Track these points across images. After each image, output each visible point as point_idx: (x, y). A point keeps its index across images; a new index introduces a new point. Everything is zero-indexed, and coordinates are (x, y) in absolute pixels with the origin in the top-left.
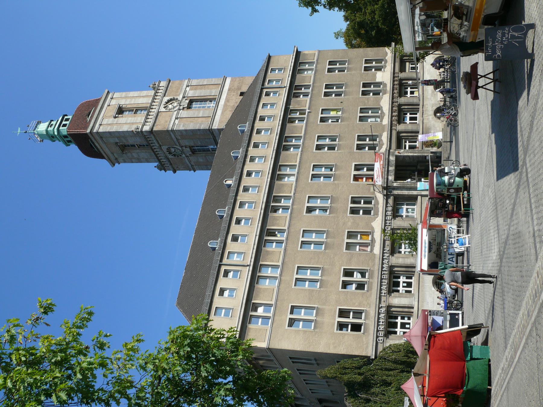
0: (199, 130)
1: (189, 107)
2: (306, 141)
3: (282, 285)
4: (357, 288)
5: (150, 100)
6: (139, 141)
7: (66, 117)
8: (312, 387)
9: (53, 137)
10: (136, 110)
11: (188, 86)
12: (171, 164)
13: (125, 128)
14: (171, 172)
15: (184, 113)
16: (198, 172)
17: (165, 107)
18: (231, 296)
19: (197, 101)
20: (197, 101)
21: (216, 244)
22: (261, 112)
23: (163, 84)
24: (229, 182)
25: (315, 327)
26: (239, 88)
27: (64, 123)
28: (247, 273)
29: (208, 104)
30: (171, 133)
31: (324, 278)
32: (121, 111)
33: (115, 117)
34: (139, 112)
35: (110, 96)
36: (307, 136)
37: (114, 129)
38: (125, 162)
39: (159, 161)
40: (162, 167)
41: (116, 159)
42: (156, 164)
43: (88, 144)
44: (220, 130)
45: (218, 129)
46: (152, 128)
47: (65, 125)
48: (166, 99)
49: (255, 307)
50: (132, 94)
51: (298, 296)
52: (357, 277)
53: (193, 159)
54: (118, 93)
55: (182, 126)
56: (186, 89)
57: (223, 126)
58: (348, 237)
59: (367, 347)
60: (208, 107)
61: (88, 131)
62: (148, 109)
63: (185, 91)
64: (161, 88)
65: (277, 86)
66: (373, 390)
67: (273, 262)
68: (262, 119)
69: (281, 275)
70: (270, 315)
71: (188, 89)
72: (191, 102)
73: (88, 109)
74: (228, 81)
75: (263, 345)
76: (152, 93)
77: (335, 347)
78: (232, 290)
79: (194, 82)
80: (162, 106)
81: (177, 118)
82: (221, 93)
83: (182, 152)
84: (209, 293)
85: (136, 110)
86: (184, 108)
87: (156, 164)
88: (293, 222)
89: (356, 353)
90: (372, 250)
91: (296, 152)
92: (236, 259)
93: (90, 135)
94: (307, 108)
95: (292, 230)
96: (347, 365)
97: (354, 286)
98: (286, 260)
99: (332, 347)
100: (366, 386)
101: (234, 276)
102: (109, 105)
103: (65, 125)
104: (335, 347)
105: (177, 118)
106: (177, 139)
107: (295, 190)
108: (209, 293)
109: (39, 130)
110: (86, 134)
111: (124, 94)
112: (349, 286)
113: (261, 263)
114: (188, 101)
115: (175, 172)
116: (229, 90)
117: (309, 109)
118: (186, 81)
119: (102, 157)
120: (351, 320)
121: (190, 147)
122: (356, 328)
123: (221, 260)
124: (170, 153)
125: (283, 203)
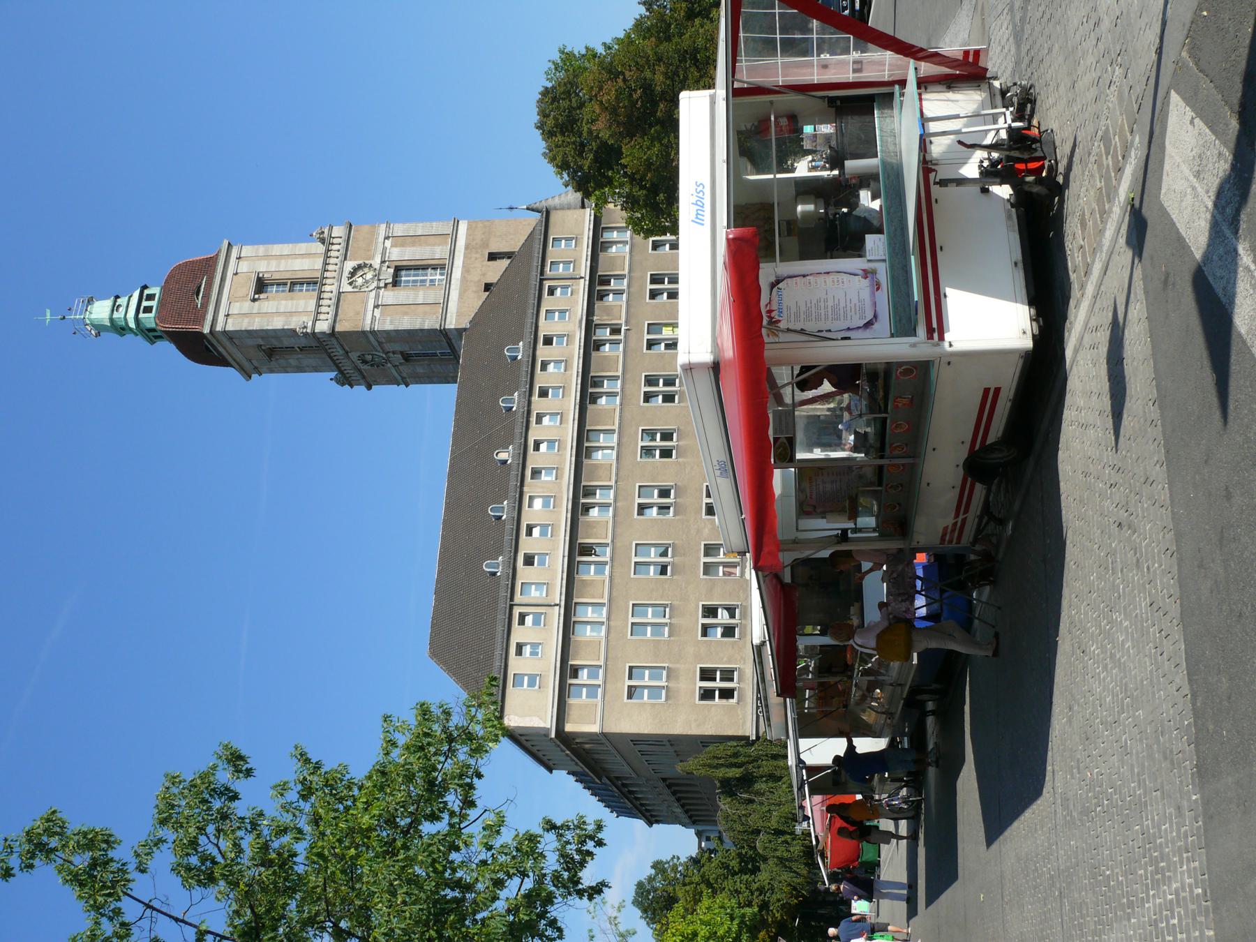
0: (422, 330)
1: (395, 283)
2: (627, 386)
3: (612, 636)
4: (723, 635)
5: (318, 264)
6: (304, 342)
7: (146, 292)
8: (648, 758)
9: (123, 329)
10: (293, 284)
11: (387, 238)
12: (364, 377)
13: (278, 324)
14: (363, 388)
15: (389, 296)
16: (412, 387)
17: (350, 284)
18: (534, 653)
19: (408, 268)
20: (408, 268)
21: (497, 565)
22: (545, 328)
23: (339, 231)
24: (503, 456)
25: (667, 698)
26: (485, 244)
27: (145, 304)
28: (556, 617)
29: (431, 275)
30: (370, 336)
31: (673, 621)
32: (261, 285)
33: (254, 300)
34: (298, 287)
35: (234, 254)
36: (628, 376)
37: (256, 324)
38: (272, 371)
39: (338, 368)
40: (345, 379)
41: (256, 368)
42: (333, 375)
43: (201, 348)
44: (460, 332)
45: (456, 330)
46: (334, 327)
47: (148, 310)
48: (349, 265)
49: (575, 672)
50: (277, 249)
51: (636, 652)
52: (723, 617)
53: (406, 370)
54: (249, 248)
55: (388, 322)
56: (386, 245)
57: (465, 324)
58: (706, 555)
59: (744, 723)
60: (432, 281)
61: (206, 330)
62: (314, 283)
63: (384, 249)
64: (335, 241)
65: (566, 274)
66: (757, 786)
67: (593, 597)
68: (548, 341)
69: (608, 619)
70: (600, 682)
71: (388, 243)
72: (398, 269)
73: (193, 280)
74: (463, 227)
75: (595, 728)
76: (321, 248)
77: (699, 725)
78: (535, 646)
79: (399, 229)
80: (345, 281)
81: (376, 306)
82: (452, 253)
83: (388, 360)
84: (498, 652)
85: (293, 284)
86: (386, 285)
87: (333, 375)
88: (619, 531)
89: (730, 733)
90: (743, 573)
91: (611, 407)
92: (535, 594)
93: (210, 337)
94: (623, 321)
95: (618, 544)
96: (719, 753)
97: (719, 631)
98: (615, 594)
99: (693, 725)
100: (746, 781)
101: (536, 622)
102: (236, 274)
103: (148, 310)
104: (699, 725)
105: (376, 306)
106: (380, 343)
107: (617, 475)
108: (498, 652)
109: (93, 316)
110: (201, 334)
111: (261, 249)
112: (647, 511)
113: (576, 600)
114: (391, 271)
115: (369, 388)
116: (467, 247)
117: (627, 323)
118: (383, 226)
119: (222, 362)
120: (718, 684)
121: (402, 353)
122: (727, 694)
123: (512, 599)
124: (365, 362)
125: (599, 497)
